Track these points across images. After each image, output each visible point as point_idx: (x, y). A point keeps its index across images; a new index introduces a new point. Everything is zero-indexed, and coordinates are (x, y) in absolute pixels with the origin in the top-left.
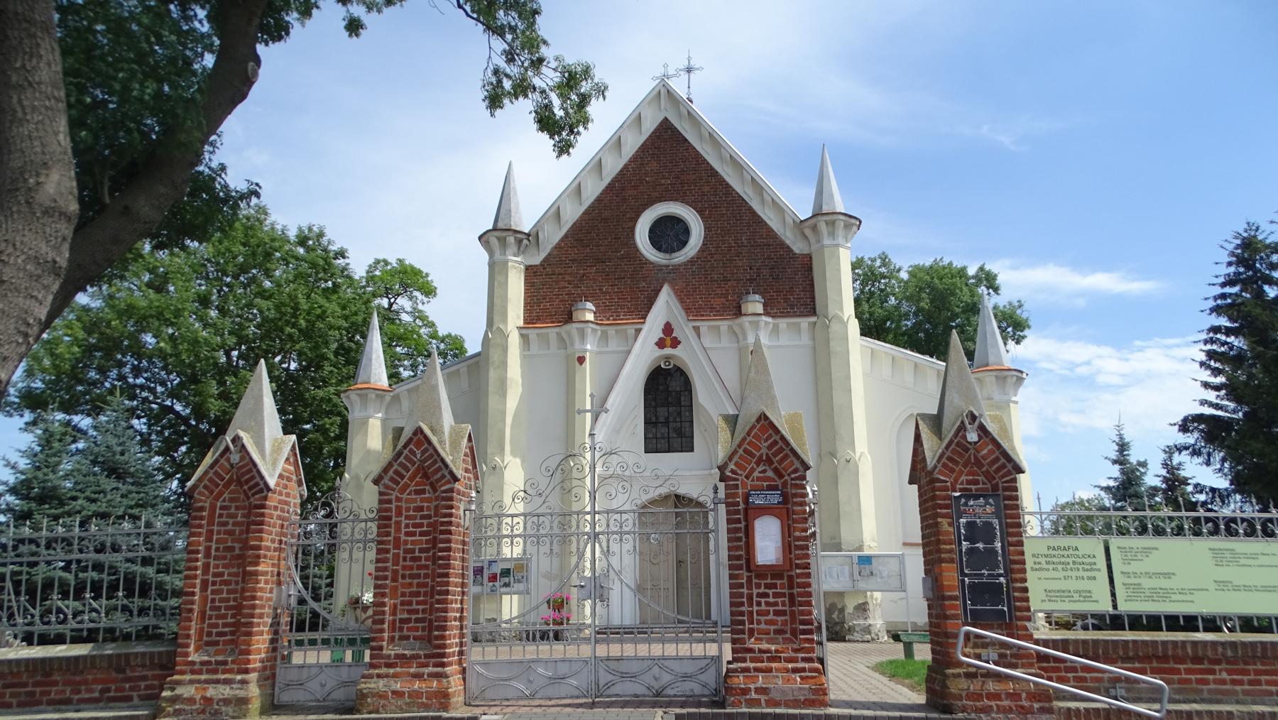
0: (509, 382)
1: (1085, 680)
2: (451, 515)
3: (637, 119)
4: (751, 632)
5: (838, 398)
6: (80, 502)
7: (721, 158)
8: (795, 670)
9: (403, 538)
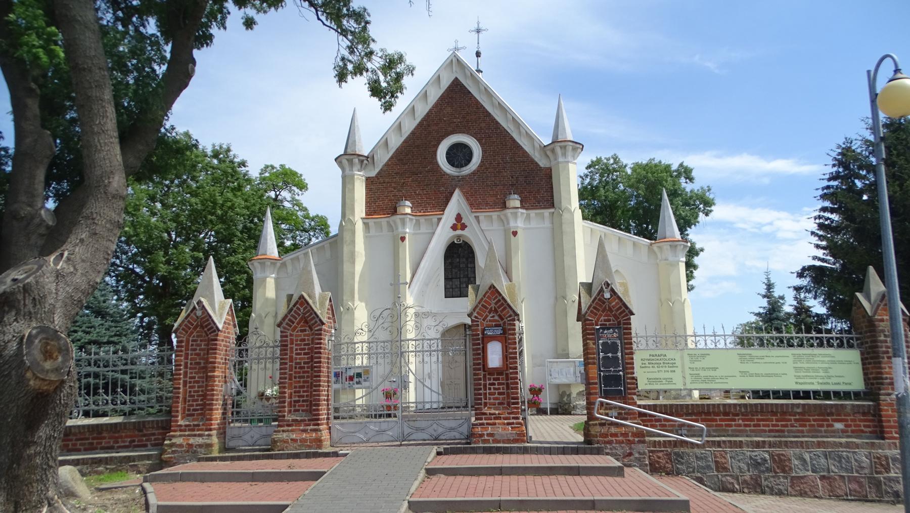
1: (665, 426)
2: (320, 343)
3: (437, 79)
4: (486, 404)
5: (567, 261)
6: (80, 333)
7: (493, 105)
8: (508, 424)
9: (294, 356)
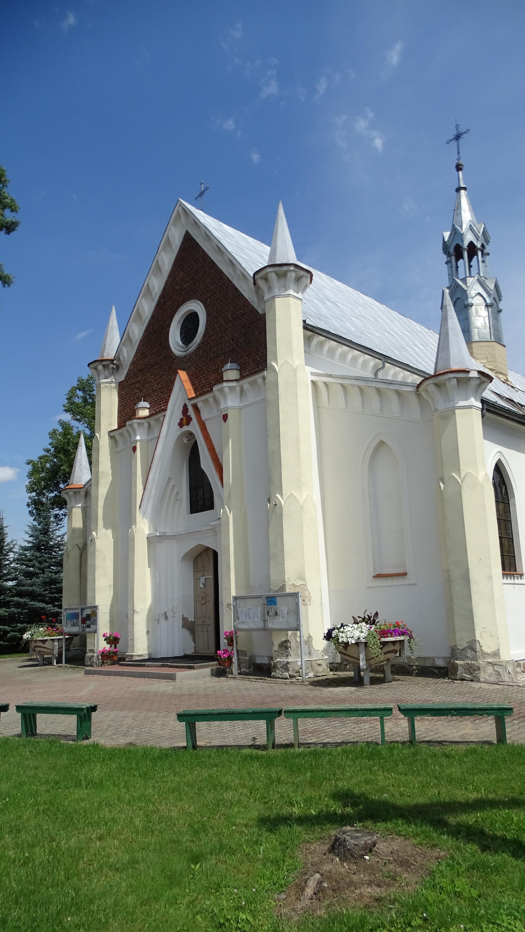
0: (100, 474)
